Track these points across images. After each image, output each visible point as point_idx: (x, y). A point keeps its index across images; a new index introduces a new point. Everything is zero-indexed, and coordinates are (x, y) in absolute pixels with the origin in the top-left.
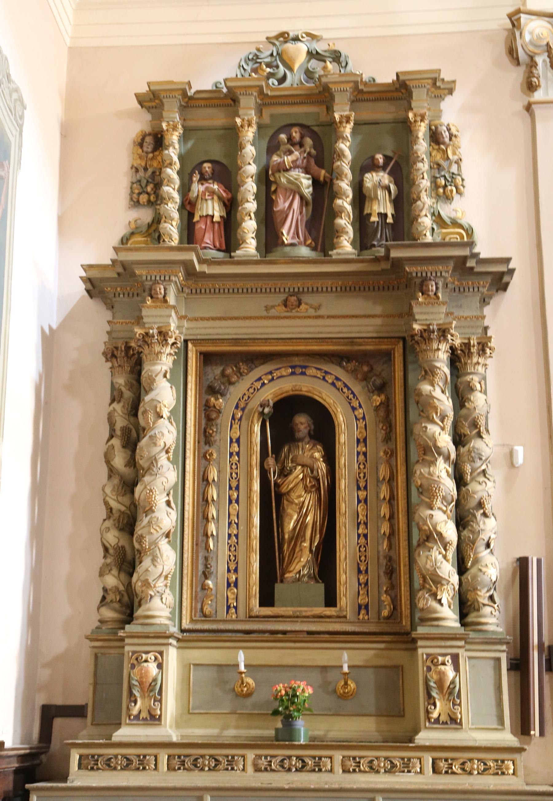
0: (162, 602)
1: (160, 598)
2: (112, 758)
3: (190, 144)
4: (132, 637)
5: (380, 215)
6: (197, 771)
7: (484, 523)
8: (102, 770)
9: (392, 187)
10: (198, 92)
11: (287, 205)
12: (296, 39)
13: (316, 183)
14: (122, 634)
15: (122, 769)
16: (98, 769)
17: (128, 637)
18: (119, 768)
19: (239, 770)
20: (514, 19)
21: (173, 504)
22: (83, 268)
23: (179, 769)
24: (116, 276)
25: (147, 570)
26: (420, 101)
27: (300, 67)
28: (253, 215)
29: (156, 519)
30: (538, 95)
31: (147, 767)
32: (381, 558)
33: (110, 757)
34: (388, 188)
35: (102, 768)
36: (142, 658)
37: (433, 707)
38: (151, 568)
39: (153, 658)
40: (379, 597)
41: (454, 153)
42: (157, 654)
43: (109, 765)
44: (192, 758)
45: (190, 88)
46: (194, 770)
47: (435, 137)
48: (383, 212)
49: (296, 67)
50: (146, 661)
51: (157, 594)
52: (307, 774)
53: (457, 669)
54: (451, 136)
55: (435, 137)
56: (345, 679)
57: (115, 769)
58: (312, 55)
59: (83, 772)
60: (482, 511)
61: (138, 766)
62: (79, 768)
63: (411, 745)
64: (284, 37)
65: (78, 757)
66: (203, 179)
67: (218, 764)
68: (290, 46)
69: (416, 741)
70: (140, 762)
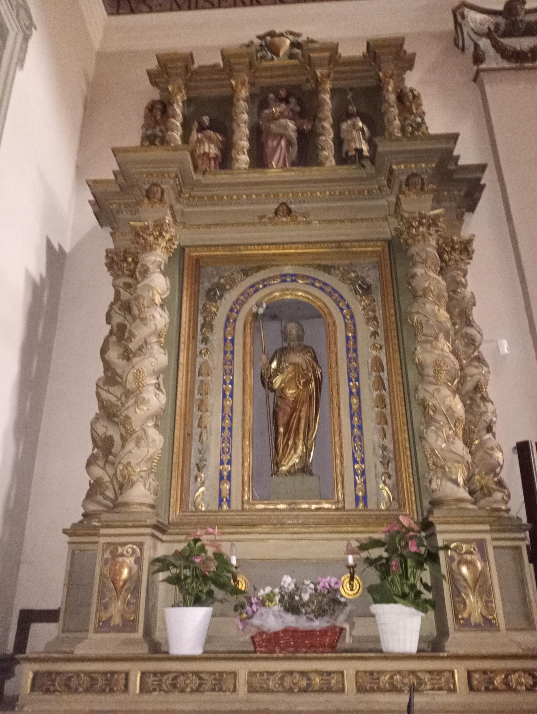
0: (145, 488)
1: (143, 483)
2: (73, 677)
3: (191, 109)
4: (108, 527)
5: (357, 150)
6: (177, 693)
7: (485, 405)
8: (59, 691)
9: (365, 129)
10: (201, 67)
11: (275, 143)
12: (282, 35)
13: (300, 132)
14: (96, 524)
15: (299, 692)
16: (55, 691)
17: (103, 527)
18: (81, 689)
19: (229, 691)
20: (458, 15)
21: (162, 387)
22: (89, 185)
23: (155, 690)
24: (118, 189)
25: (130, 452)
26: (388, 67)
27: (285, 53)
28: (245, 151)
29: (141, 399)
30: (483, 66)
31: (115, 689)
32: (377, 447)
33: (71, 675)
34: (362, 130)
35: (60, 690)
36: (117, 551)
37: (462, 606)
38: (135, 451)
39: (130, 550)
40: (378, 487)
41: (417, 109)
42: (135, 547)
43: (68, 686)
44: (172, 676)
45: (193, 62)
46: (173, 692)
47: (401, 97)
48: (358, 147)
49: (282, 53)
50: (122, 555)
51: (141, 480)
52: (313, 695)
53: (484, 558)
54: (414, 96)
55: (401, 97)
56: (350, 573)
57: (76, 691)
58: (294, 45)
59: (38, 696)
60: (479, 395)
61: (104, 687)
62: (33, 689)
63: (442, 654)
64: (272, 34)
65: (31, 675)
66: (201, 129)
67: (203, 684)
68: (277, 40)
69: (446, 649)
70: (108, 682)
